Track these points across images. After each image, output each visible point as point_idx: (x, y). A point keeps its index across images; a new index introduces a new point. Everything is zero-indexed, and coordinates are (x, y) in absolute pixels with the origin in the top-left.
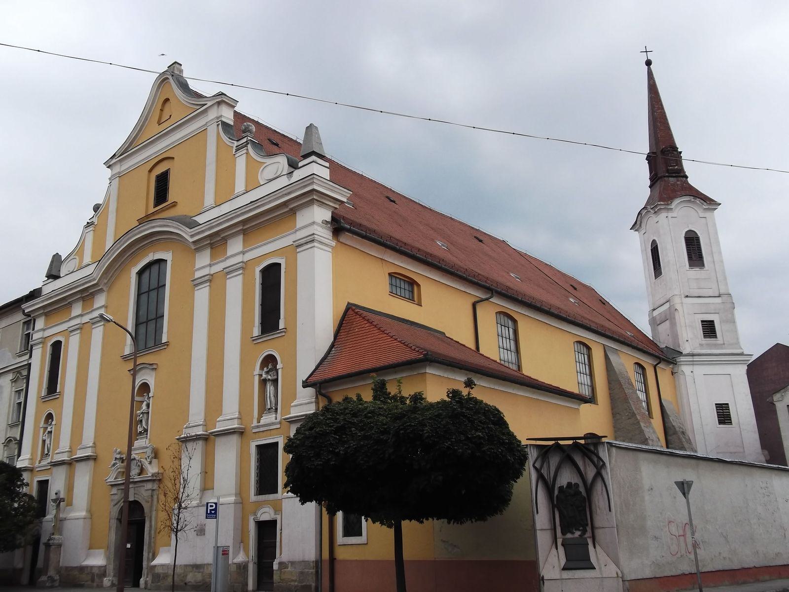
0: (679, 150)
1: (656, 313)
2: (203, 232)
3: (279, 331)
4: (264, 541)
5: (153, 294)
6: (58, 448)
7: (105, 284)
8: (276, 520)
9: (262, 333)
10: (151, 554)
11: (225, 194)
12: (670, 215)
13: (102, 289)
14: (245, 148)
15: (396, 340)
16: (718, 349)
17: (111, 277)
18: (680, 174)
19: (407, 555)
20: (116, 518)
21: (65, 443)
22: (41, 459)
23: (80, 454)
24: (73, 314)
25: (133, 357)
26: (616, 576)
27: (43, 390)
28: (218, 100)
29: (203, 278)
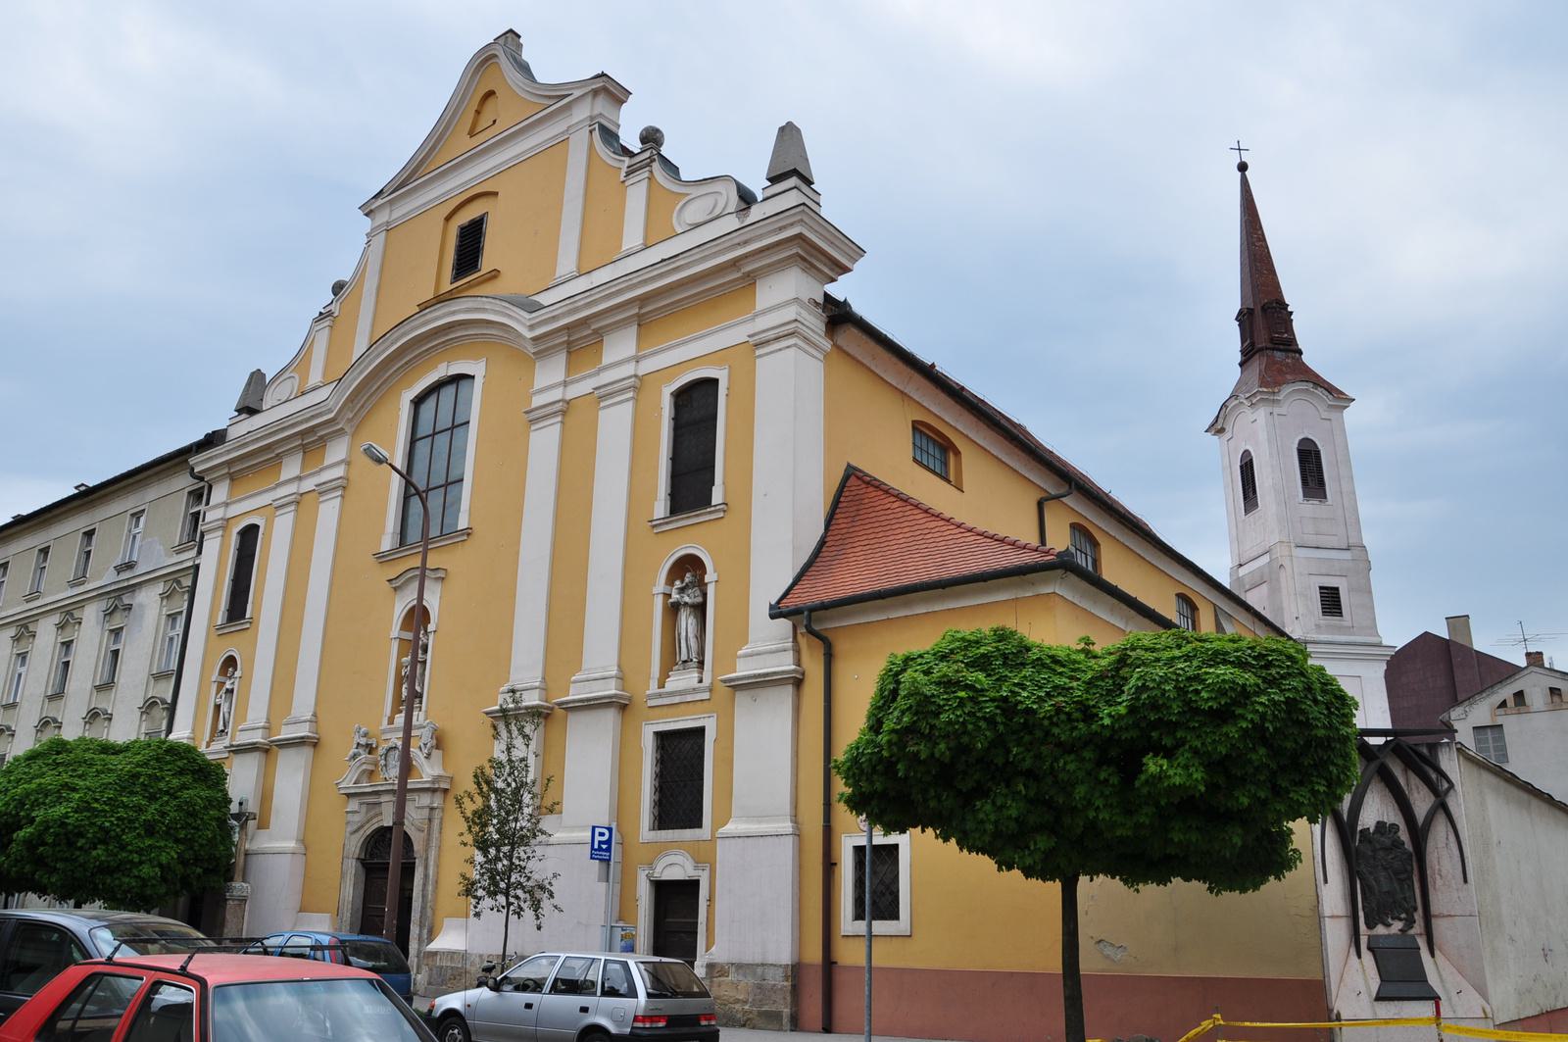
0: (1289, 309)
1: (1242, 571)
2: (554, 318)
3: (713, 509)
4: (667, 920)
5: (442, 440)
7: (350, 420)
8: (698, 881)
9: (671, 513)
10: (425, 931)
12: (1277, 410)
13: (342, 429)
14: (647, 169)
17: (362, 406)
18: (1290, 346)
20: (356, 856)
22: (211, 740)
23: (286, 733)
24: (284, 476)
25: (421, 549)
27: (221, 613)
28: (594, 87)
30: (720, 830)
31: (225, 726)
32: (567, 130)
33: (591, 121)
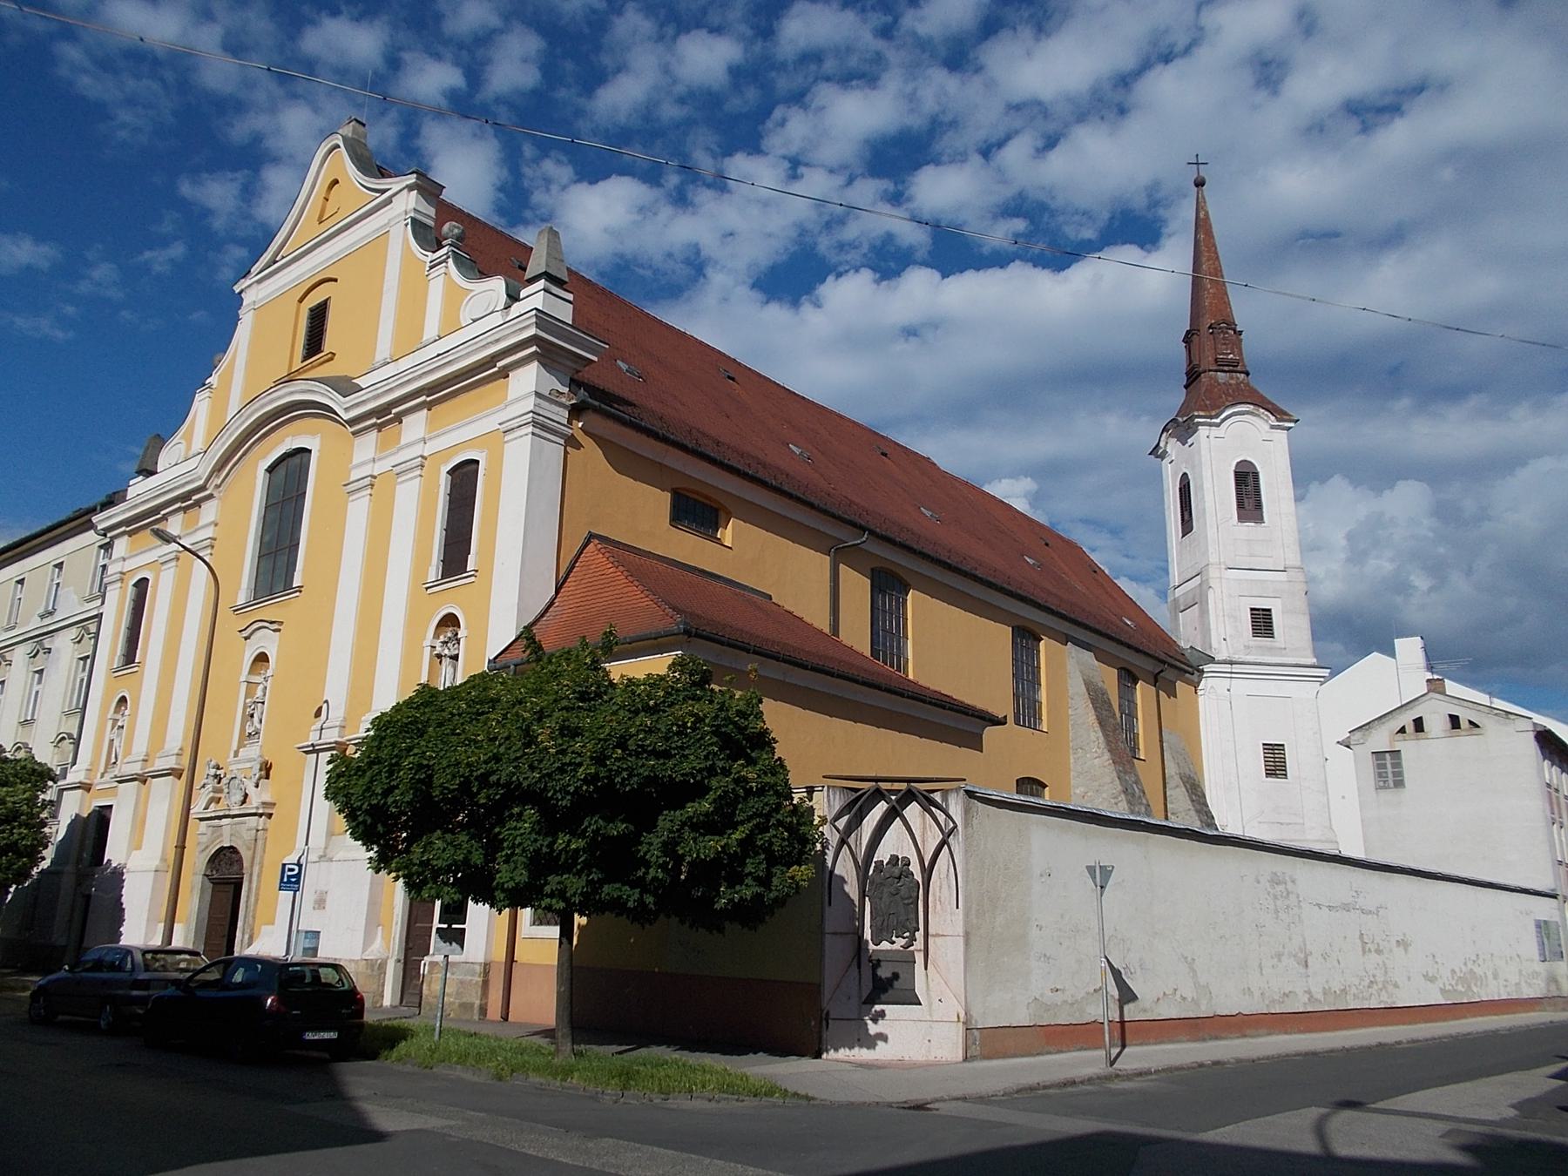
7: (218, 486)
11: (409, 338)
14: (444, 264)
15: (647, 597)
16: (1276, 656)
19: (574, 965)
21: (140, 746)
26: (956, 1020)
28: (408, 182)
29: (361, 481)
31: (116, 758)
32: (388, 223)
33: (406, 214)
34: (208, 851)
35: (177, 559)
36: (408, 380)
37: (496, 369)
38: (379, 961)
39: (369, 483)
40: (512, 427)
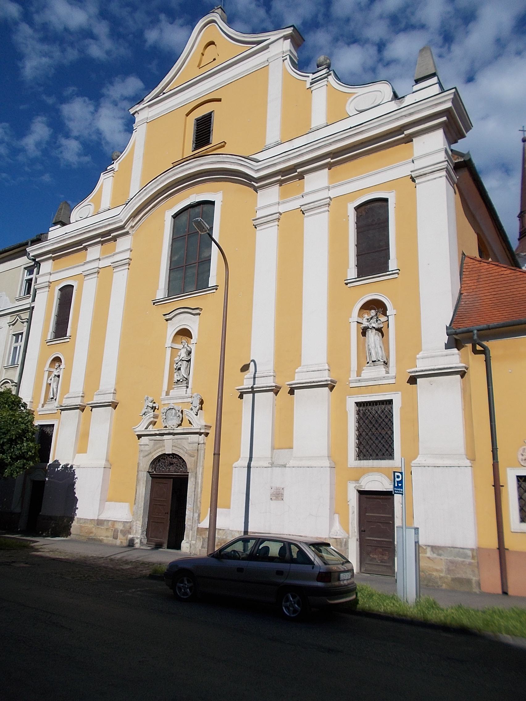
6: (68, 392)
7: (132, 227)
14: (326, 79)
23: (97, 399)
30: (413, 462)
34: (150, 456)
35: (98, 273)
36: (84, 232)
37: (403, 136)
38: (345, 540)
39: (277, 217)
40: (425, 172)
